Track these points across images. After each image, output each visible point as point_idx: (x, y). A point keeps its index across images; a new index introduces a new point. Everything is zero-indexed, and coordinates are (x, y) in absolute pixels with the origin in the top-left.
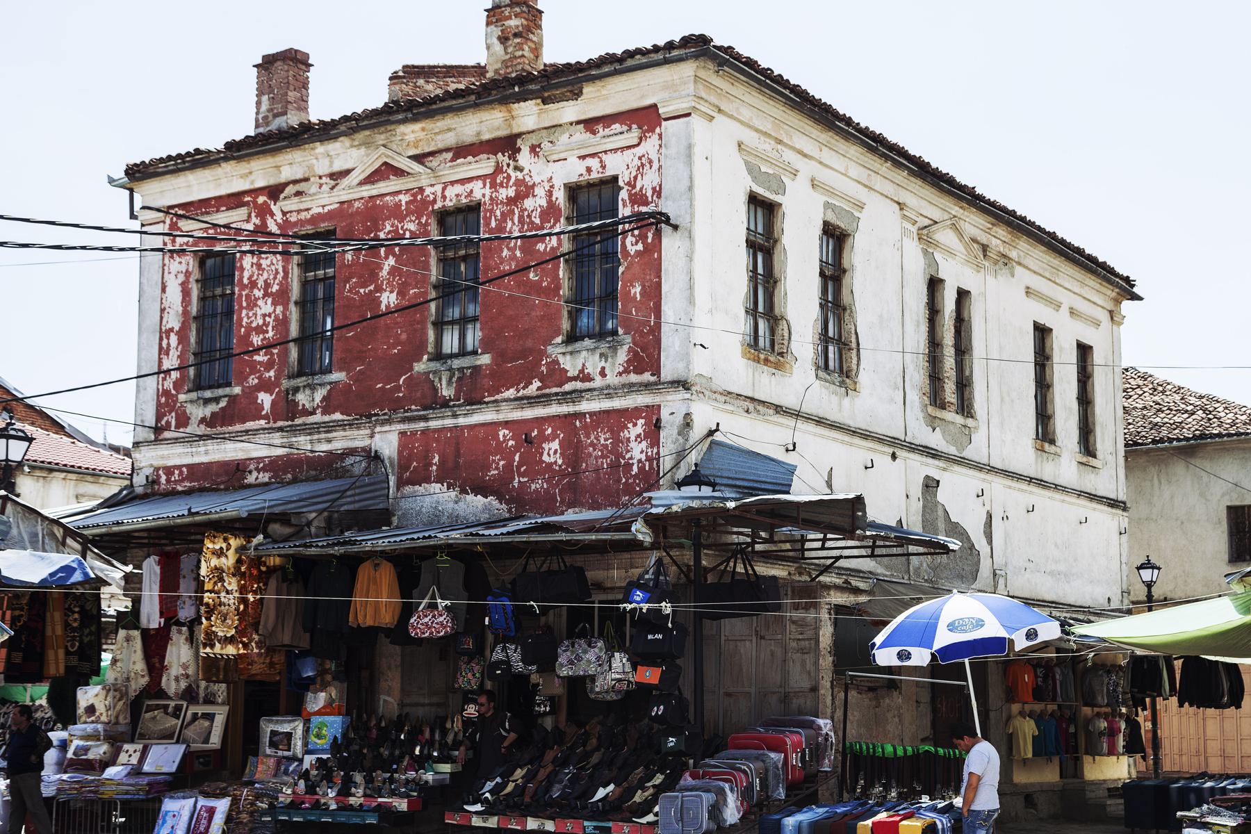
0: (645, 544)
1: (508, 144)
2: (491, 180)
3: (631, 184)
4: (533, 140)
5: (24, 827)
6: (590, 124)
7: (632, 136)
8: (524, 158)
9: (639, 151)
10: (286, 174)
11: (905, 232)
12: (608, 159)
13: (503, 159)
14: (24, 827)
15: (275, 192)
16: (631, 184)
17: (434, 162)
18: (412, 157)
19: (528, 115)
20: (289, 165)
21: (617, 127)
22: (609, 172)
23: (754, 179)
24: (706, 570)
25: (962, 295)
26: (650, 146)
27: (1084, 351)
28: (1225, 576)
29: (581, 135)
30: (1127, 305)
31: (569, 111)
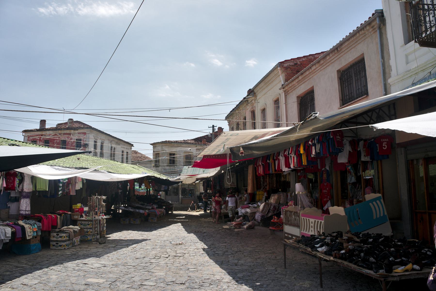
0: (316, 236)
1: (70, 134)
2: (68, 137)
3: (83, 140)
4: (73, 134)
5: (314, 181)
6: (79, 133)
7: (83, 135)
8: (71, 136)
9: (84, 137)
10: (43, 134)
11: (109, 142)
12: (81, 137)
13: (69, 135)
14: (314, 181)
15: (42, 135)
16: (83, 140)
17: (61, 135)
18: (59, 134)
19: (72, 131)
20: (44, 133)
21: (82, 134)
22: (81, 138)
23: (95, 139)
24: (123, 206)
25: (114, 148)
26: (85, 136)
27: (127, 153)
28: (312, 232)
29: (78, 134)
30: (132, 147)
31: (77, 132)
